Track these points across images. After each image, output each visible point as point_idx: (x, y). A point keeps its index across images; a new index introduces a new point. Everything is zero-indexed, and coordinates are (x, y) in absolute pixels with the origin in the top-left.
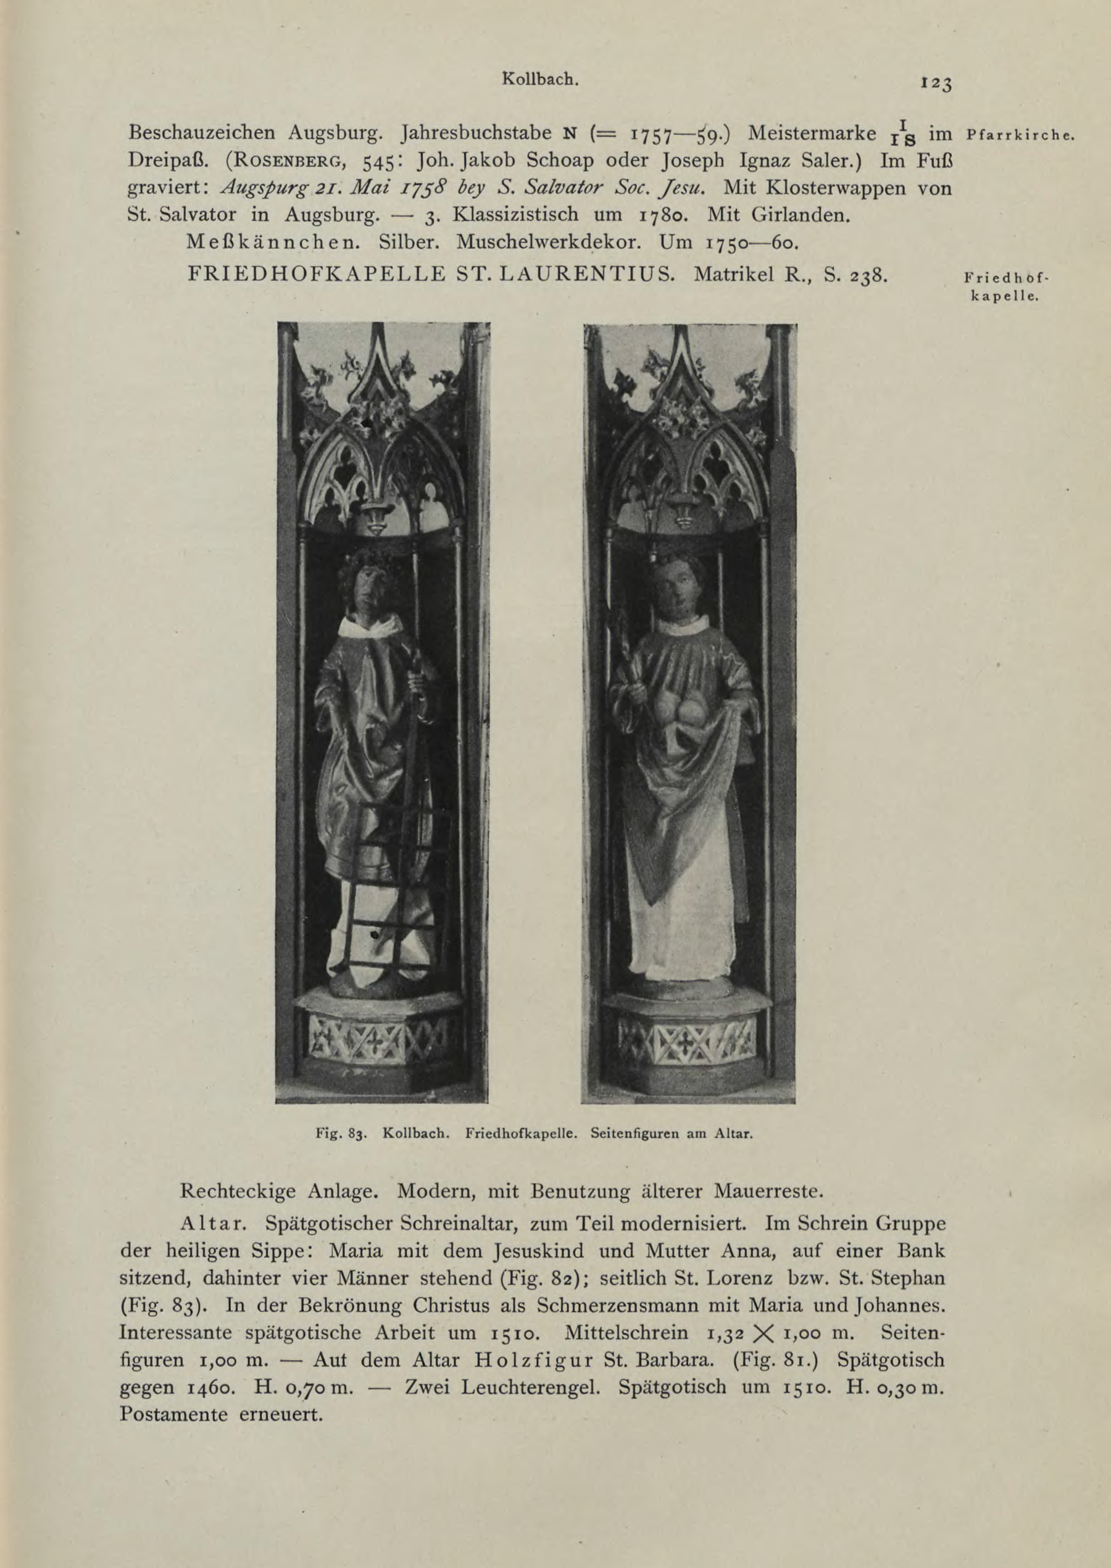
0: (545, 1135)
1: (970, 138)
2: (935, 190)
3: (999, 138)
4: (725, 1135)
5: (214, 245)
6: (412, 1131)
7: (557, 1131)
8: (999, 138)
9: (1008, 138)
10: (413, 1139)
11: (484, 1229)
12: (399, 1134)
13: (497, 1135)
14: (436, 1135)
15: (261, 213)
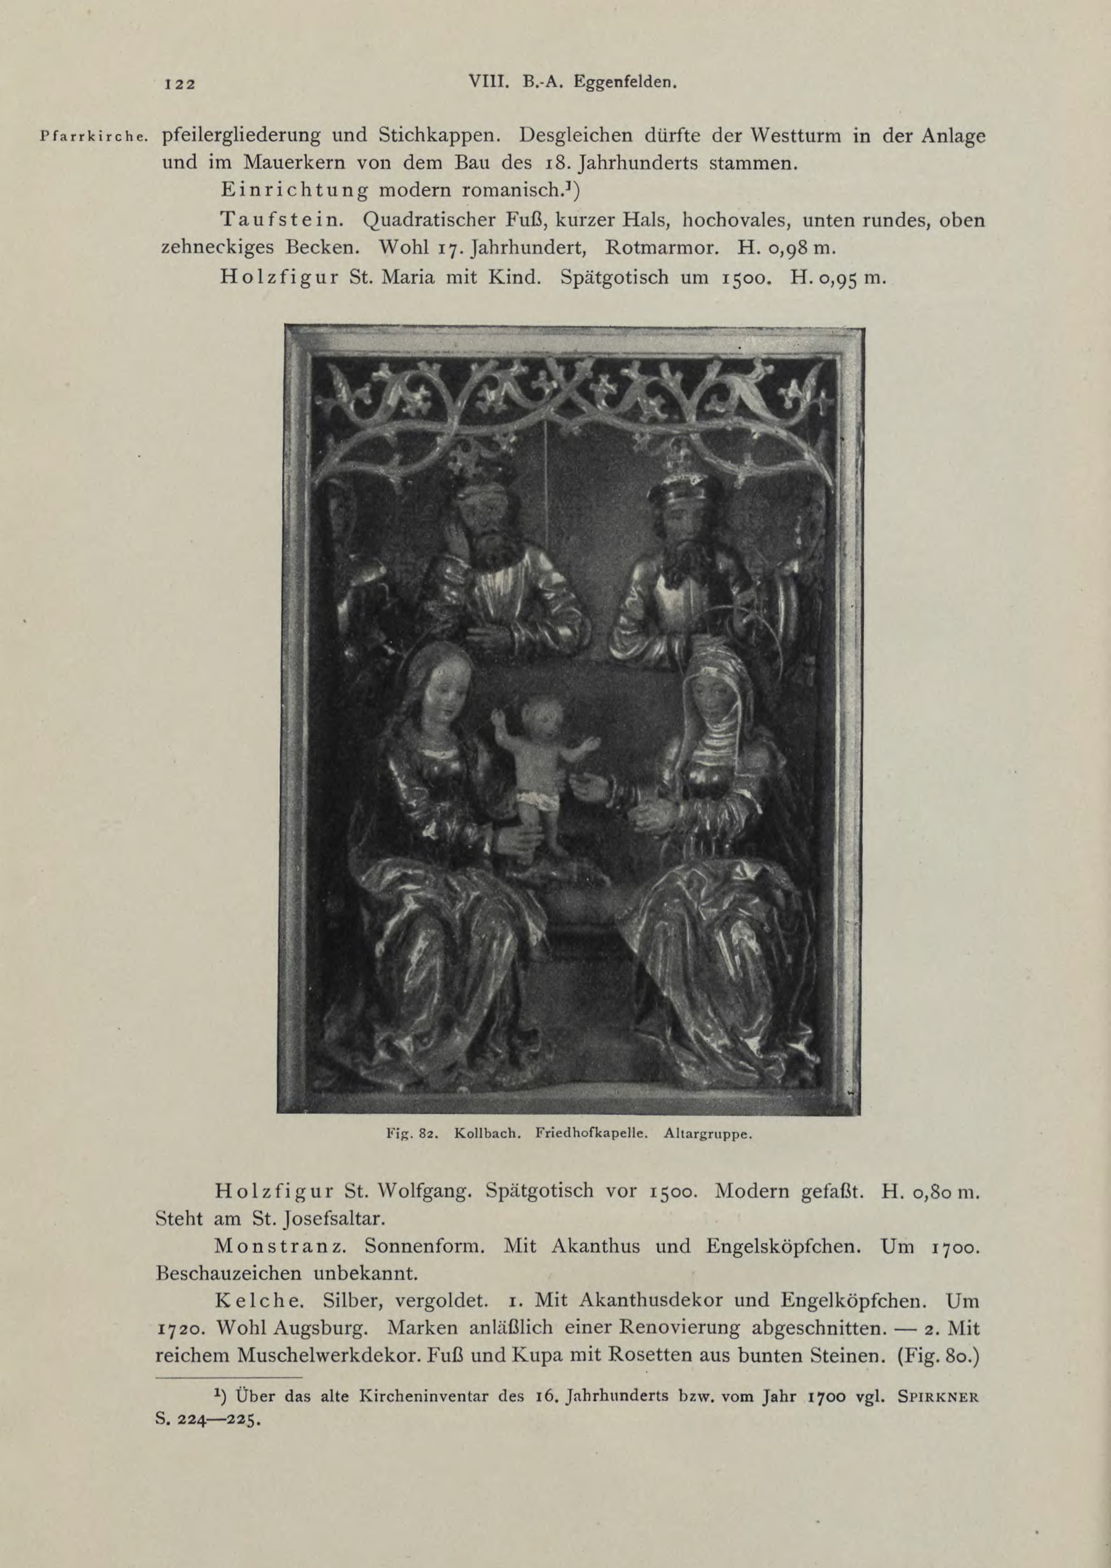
0: (615, 1134)
1: (43, 139)
2: (374, 164)
3: (73, 140)
4: (675, 1134)
5: (307, 223)
6: (483, 1131)
7: (627, 1131)
8: (73, 140)
9: (81, 140)
10: (484, 1139)
11: (352, 1224)
12: (471, 1135)
13: (567, 1134)
14: (508, 1134)
15: (862, 135)
